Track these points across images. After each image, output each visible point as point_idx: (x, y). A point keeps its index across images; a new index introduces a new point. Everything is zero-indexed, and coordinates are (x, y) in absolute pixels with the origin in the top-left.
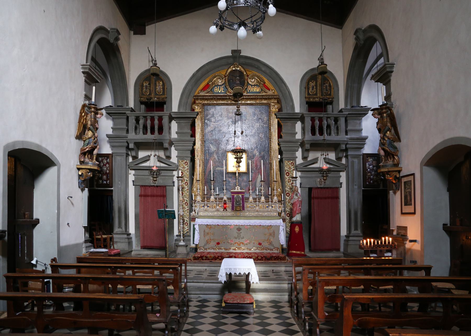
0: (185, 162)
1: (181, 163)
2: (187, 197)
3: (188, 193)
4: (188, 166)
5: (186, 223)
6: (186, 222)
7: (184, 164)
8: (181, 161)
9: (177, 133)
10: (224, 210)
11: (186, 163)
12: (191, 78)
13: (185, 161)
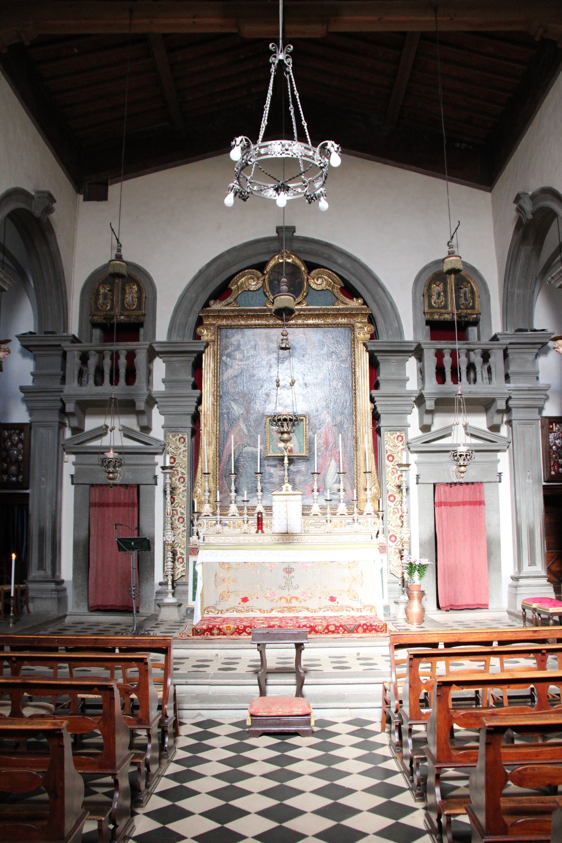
0: (180, 438)
1: (171, 440)
2: (183, 546)
3: (185, 499)
4: (186, 485)
5: (179, 558)
6: (179, 555)
7: (178, 442)
8: (171, 437)
9: (164, 381)
10: (257, 532)
11: (182, 440)
12: (195, 279)
13: (180, 435)
